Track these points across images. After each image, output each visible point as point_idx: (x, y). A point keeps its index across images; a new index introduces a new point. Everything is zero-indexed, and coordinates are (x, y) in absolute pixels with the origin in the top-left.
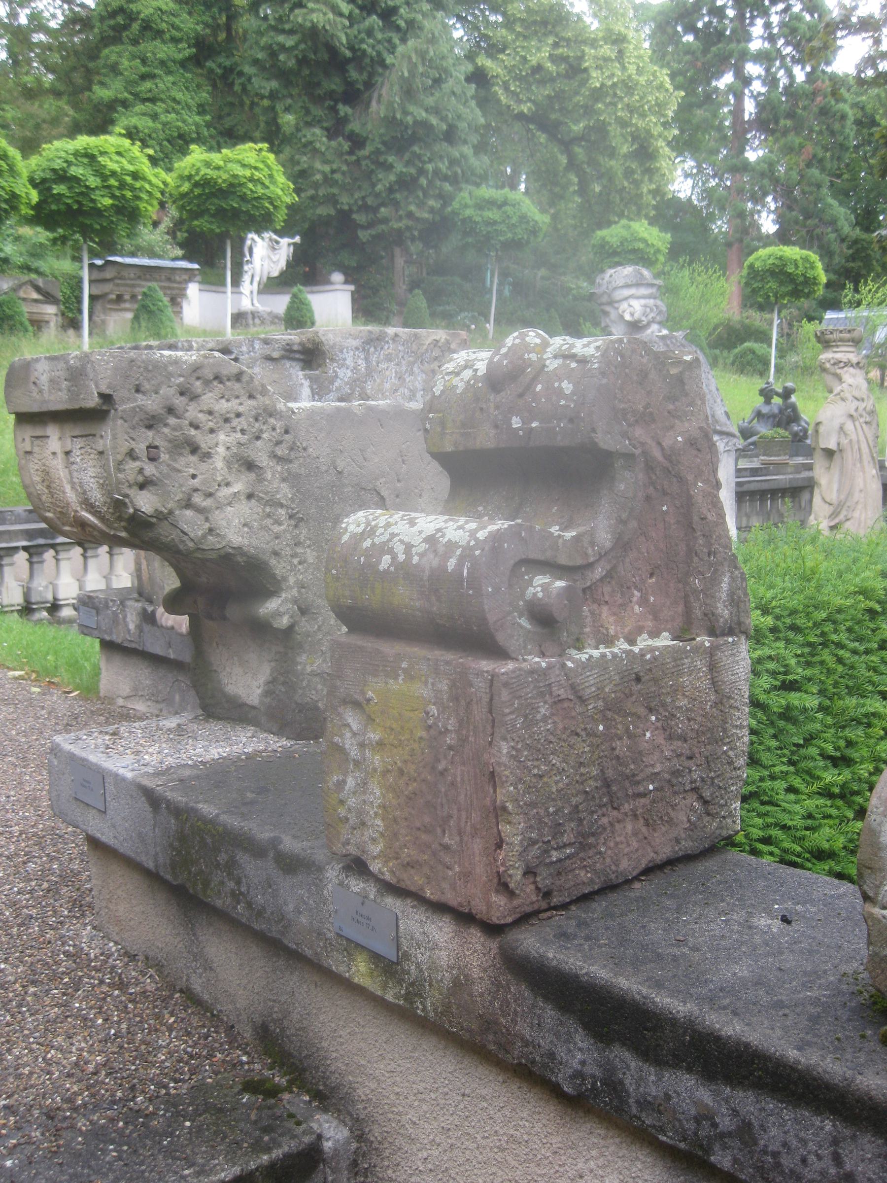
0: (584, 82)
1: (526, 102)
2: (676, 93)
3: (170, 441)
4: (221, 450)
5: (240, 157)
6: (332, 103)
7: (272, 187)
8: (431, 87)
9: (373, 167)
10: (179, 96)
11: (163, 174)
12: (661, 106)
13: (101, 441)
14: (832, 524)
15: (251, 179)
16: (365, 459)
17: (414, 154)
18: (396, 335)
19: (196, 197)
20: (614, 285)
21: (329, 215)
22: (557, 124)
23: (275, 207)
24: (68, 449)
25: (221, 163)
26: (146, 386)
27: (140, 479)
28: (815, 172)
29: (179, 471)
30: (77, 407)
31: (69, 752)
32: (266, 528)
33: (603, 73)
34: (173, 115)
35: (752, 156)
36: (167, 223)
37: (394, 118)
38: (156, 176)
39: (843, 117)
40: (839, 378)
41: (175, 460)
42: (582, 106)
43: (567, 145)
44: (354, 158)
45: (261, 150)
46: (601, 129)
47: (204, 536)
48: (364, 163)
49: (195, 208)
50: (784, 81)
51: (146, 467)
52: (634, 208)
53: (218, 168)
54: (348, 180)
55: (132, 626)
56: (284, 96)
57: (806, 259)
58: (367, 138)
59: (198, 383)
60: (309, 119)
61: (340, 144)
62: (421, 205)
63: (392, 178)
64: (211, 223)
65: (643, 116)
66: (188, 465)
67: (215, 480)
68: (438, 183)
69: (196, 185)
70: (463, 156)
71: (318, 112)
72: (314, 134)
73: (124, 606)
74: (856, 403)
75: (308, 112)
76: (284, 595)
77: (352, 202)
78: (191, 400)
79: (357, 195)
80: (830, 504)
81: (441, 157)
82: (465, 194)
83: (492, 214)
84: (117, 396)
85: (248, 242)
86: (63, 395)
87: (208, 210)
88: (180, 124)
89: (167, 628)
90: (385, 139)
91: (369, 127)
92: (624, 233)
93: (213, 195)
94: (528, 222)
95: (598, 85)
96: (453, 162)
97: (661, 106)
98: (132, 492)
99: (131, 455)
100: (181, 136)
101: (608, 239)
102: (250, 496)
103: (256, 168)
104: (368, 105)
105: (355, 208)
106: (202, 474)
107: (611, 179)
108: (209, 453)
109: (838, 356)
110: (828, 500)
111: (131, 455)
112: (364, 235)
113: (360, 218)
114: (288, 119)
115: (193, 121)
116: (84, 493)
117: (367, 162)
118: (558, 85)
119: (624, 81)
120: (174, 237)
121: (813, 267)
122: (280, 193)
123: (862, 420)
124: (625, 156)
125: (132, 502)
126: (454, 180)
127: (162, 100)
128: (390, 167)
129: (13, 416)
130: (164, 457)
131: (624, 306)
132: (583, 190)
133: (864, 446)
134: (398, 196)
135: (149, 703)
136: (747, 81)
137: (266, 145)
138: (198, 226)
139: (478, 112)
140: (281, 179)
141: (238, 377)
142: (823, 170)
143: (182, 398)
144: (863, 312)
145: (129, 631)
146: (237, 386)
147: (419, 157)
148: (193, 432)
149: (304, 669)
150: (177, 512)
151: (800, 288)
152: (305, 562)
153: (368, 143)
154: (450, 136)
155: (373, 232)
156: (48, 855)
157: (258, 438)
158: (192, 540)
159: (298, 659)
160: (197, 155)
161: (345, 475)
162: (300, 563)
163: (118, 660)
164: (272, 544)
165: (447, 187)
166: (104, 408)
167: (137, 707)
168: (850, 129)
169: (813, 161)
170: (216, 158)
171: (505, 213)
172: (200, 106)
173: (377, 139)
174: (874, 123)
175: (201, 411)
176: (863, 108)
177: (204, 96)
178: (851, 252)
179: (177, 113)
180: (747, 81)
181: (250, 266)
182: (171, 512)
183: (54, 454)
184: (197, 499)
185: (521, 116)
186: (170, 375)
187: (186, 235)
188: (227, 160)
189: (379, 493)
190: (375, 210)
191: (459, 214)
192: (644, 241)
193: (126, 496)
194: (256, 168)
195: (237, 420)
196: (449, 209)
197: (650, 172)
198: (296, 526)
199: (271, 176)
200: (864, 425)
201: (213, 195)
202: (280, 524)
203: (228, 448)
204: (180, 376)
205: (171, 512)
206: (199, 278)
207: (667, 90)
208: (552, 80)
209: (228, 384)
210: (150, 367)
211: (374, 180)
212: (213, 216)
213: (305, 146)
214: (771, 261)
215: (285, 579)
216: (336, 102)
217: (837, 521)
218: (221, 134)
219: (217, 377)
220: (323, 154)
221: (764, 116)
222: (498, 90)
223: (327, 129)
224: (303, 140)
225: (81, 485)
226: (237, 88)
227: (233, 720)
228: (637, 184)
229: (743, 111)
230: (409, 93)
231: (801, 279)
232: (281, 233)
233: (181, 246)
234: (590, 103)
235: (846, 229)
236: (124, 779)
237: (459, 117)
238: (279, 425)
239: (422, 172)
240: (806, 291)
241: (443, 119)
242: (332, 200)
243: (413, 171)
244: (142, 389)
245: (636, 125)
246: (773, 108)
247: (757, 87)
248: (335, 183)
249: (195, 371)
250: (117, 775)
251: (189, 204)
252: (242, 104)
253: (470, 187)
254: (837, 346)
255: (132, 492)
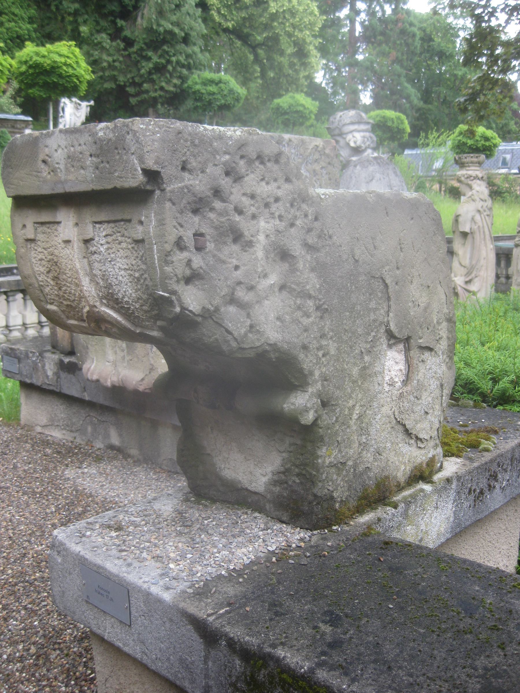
0: (266, 10)
1: (230, 21)
2: (321, 17)
3: (216, 228)
4: (261, 237)
5: (58, 50)
6: (113, 18)
7: (78, 69)
8: (175, 10)
9: (139, 59)
10: (17, 11)
11: (10, 60)
12: (312, 24)
13: (140, 228)
14: (467, 279)
15: (65, 64)
16: (375, 247)
17: (164, 51)
18: (290, 140)
19: (30, 75)
20: (343, 122)
21: (112, 88)
22: (248, 35)
23: (80, 82)
24: (88, 237)
25: (46, 54)
26: (193, 163)
27: (188, 272)
28: (397, 67)
29: (224, 262)
30: (109, 186)
31: (78, 555)
32: (296, 321)
33: (277, 4)
34: (13, 24)
35: (360, 57)
36: (10, 92)
37: (152, 28)
38: (5, 60)
39: (414, 35)
40: (470, 187)
41: (219, 250)
42: (264, 24)
43: (254, 48)
44: (127, 53)
45: (70, 46)
46: (275, 39)
47: (246, 334)
48: (133, 56)
49: (30, 82)
50: (379, 14)
51: (194, 259)
52: (294, 86)
53: (44, 57)
54: (123, 66)
55: (50, 373)
56: (83, 13)
57: (398, 118)
58: (135, 41)
59: (242, 163)
60: (98, 28)
61: (118, 44)
62: (168, 82)
63: (151, 65)
64: (40, 91)
65: (301, 31)
66: (231, 256)
67: (256, 272)
68: (179, 69)
69: (30, 67)
70: (194, 53)
71: (104, 23)
72: (102, 38)
73: (42, 357)
74: (482, 203)
75: (98, 23)
76: (310, 390)
77: (126, 80)
78: (235, 181)
79: (129, 76)
80: (465, 267)
81: (181, 53)
82: (195, 76)
83: (212, 88)
84: (166, 173)
85: (62, 105)
86: (89, 174)
87: (38, 83)
88: (18, 29)
89: (92, 381)
90: (147, 41)
91: (136, 34)
92: (291, 101)
93: (41, 73)
94: (234, 94)
95: (274, 11)
96: (188, 56)
97: (312, 24)
98: (180, 288)
99: (180, 245)
100: (18, 37)
101: (281, 104)
102: (282, 288)
103: (68, 57)
104: (135, 20)
105: (128, 84)
106: (244, 265)
107: (280, 70)
108: (251, 242)
109: (470, 173)
110: (463, 264)
111: (180, 245)
112: (133, 101)
113: (131, 90)
114: (84, 29)
115: (26, 27)
116: (109, 286)
117: (135, 55)
118: (250, 11)
119: (289, 9)
120: (15, 101)
121: (402, 123)
122: (83, 73)
123: (485, 214)
124: (289, 55)
125: (179, 300)
126: (189, 67)
127: (6, 14)
128: (149, 59)
129: (10, 200)
130: (210, 246)
131: (349, 137)
132: (263, 75)
133: (486, 230)
134: (154, 77)
135: (64, 432)
136: (358, 13)
137: (74, 43)
138: (32, 93)
139: (203, 26)
140: (83, 64)
141: (277, 158)
142: (402, 66)
143: (227, 179)
144: (429, 150)
145: (47, 377)
146: (276, 167)
147: (167, 53)
148: (237, 218)
149: (324, 462)
150: (223, 309)
151: (395, 135)
152: (328, 354)
153: (136, 44)
154: (186, 40)
155: (139, 99)
156: (25, 608)
157: (292, 225)
158: (236, 339)
159: (319, 453)
160: (30, 49)
161: (361, 262)
162: (324, 355)
163: (35, 398)
164: (301, 338)
165: (185, 71)
166: (149, 187)
167: (54, 434)
168: (418, 43)
169: (397, 61)
170: (42, 50)
171: (220, 88)
172: (30, 18)
173: (142, 42)
174: (431, 40)
175: (244, 194)
176: (424, 31)
177: (33, 12)
178: (418, 115)
179: (16, 22)
180: (358, 13)
181: (63, 119)
182: (217, 309)
183: (67, 242)
184: (241, 293)
185: (226, 30)
186: (215, 152)
187: (22, 99)
188: (50, 52)
189: (384, 281)
190: (140, 85)
191: (191, 88)
192: (303, 106)
193: (174, 292)
194: (68, 57)
195: (276, 205)
196: (186, 85)
197: (305, 65)
198: (321, 317)
199: (77, 63)
200: (486, 217)
201: (41, 73)
202: (308, 316)
203: (267, 236)
204: (226, 153)
205: (217, 309)
206: (31, 126)
207: (316, 16)
208: (247, 8)
209: (269, 165)
210: (197, 141)
211: (139, 67)
212: (41, 87)
213: (96, 45)
214: (378, 119)
215: (311, 373)
216: (116, 18)
217: (470, 278)
218: (43, 36)
219: (259, 157)
220: (108, 50)
221: (368, 33)
222: (214, 13)
223: (110, 35)
224: (96, 41)
225: (104, 277)
226: (53, 8)
227: (229, 503)
228: (296, 71)
229: (355, 31)
230: (161, 13)
231: (396, 130)
232: (82, 99)
233: (21, 106)
234: (269, 22)
235: (416, 101)
236: (159, 601)
237: (191, 29)
238: (311, 211)
239: (169, 62)
240: (399, 137)
241: (182, 29)
242: (114, 79)
243: (163, 61)
244: (189, 166)
245: (297, 36)
246: (373, 29)
247: (363, 16)
248: (115, 68)
249: (239, 148)
250: (148, 594)
251: (26, 79)
252: (56, 19)
253: (198, 72)
254: (469, 166)
255: (180, 288)
